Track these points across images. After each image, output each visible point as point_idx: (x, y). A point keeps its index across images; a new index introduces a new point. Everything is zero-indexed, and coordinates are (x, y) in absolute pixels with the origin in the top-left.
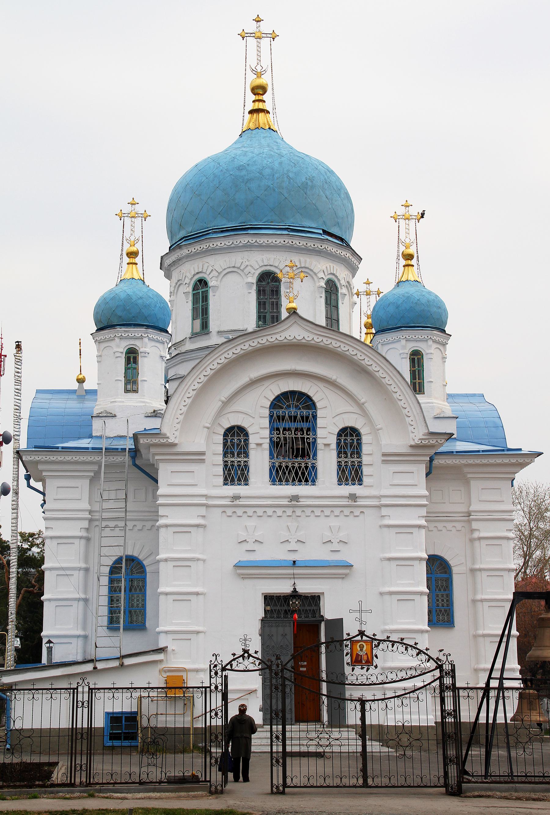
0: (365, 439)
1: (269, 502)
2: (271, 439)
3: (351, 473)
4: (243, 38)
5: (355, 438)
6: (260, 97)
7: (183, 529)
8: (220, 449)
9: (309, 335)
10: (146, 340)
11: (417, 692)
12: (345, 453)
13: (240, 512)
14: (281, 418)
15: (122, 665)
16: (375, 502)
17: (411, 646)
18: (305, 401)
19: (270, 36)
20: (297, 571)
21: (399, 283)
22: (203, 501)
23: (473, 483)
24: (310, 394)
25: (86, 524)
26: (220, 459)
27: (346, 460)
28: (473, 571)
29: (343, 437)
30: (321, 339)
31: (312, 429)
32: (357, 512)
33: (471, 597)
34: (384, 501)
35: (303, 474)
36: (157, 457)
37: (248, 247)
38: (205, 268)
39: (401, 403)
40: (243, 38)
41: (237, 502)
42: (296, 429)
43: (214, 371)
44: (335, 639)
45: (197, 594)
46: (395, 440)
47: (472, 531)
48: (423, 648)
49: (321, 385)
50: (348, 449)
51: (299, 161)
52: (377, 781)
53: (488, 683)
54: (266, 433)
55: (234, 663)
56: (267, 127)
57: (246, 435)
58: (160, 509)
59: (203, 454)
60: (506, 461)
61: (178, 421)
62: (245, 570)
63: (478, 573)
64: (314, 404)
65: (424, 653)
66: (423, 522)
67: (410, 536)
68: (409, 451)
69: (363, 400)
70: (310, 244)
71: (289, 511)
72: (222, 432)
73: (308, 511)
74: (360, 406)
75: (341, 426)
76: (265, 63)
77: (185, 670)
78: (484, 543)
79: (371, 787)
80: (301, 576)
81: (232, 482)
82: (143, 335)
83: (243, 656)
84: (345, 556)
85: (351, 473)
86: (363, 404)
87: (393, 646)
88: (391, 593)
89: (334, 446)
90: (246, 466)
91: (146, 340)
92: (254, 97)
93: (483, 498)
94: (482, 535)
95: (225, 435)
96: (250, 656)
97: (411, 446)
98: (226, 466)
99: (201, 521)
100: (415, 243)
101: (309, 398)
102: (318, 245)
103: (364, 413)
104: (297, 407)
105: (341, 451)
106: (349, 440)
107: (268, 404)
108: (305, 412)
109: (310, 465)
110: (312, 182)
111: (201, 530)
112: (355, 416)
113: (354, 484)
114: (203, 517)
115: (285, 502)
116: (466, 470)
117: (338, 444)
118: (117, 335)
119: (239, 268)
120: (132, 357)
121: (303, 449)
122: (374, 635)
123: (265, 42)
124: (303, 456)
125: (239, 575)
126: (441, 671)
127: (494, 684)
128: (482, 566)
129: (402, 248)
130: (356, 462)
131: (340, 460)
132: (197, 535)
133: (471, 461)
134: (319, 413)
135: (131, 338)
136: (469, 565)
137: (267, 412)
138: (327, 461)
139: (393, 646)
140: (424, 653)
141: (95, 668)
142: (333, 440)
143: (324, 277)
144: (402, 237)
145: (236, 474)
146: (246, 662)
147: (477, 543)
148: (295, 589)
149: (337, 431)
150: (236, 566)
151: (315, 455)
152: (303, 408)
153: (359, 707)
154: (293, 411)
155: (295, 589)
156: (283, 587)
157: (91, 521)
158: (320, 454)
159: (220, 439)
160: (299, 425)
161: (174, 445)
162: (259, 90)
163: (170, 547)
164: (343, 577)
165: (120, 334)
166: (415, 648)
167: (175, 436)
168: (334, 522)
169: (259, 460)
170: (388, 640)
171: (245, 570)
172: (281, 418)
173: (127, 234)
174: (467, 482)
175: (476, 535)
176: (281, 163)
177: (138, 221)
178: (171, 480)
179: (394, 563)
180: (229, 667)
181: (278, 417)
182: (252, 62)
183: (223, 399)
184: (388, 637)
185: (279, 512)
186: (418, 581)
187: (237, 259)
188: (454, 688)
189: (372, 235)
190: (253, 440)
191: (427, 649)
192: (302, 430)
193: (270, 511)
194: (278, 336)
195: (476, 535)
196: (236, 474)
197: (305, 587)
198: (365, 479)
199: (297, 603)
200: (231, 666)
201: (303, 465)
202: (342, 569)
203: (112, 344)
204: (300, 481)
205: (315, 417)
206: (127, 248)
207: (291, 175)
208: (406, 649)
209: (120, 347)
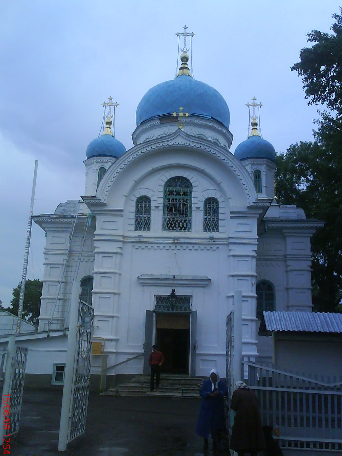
3: (211, 224)
4: (178, 36)
6: (185, 62)
7: (108, 255)
8: (133, 209)
9: (187, 142)
12: (209, 213)
13: (143, 246)
14: (170, 193)
16: (225, 242)
18: (185, 182)
19: (191, 35)
20: (175, 282)
21: (248, 138)
26: (133, 215)
27: (209, 217)
32: (214, 247)
34: (231, 241)
35: (183, 225)
38: (150, 137)
39: (242, 182)
40: (178, 36)
43: (130, 162)
47: (287, 266)
49: (195, 173)
50: (210, 211)
54: (162, 200)
56: (188, 75)
59: (121, 210)
61: (107, 190)
62: (145, 281)
70: (204, 122)
71: (173, 247)
73: (185, 246)
74: (218, 185)
77: (103, 339)
81: (140, 229)
82: (108, 160)
85: (211, 224)
86: (220, 184)
89: (202, 208)
97: (249, 208)
98: (137, 220)
99: (119, 251)
100: (258, 118)
101: (188, 180)
103: (221, 190)
104: (180, 186)
105: (207, 211)
106: (211, 205)
108: (185, 189)
109: (187, 220)
111: (119, 256)
112: (217, 191)
115: (170, 241)
116: (284, 231)
117: (205, 207)
118: (95, 160)
121: (183, 211)
123: (188, 38)
124: (183, 214)
125: (141, 283)
129: (251, 121)
130: (215, 219)
134: (194, 189)
135: (102, 162)
137: (162, 189)
138: (197, 218)
141: (48, 336)
142: (201, 205)
144: (252, 115)
145: (143, 223)
150: (139, 278)
151: (191, 213)
154: (178, 189)
156: (166, 292)
158: (193, 213)
159: (134, 203)
161: (104, 205)
162: (185, 59)
164: (204, 286)
165: (96, 160)
167: (104, 199)
169: (157, 217)
172: (170, 193)
173: (107, 113)
174: (284, 238)
175: (289, 268)
176: (190, 84)
178: (103, 226)
179: (236, 278)
181: (169, 192)
182: (182, 46)
183: (136, 180)
185: (167, 246)
186: (249, 290)
190: (153, 204)
193: (161, 246)
195: (289, 268)
196: (143, 223)
197: (180, 292)
198: (220, 229)
199: (174, 300)
201: (183, 220)
203: (93, 166)
204: (181, 229)
205: (191, 192)
206: (106, 120)
209: (96, 167)
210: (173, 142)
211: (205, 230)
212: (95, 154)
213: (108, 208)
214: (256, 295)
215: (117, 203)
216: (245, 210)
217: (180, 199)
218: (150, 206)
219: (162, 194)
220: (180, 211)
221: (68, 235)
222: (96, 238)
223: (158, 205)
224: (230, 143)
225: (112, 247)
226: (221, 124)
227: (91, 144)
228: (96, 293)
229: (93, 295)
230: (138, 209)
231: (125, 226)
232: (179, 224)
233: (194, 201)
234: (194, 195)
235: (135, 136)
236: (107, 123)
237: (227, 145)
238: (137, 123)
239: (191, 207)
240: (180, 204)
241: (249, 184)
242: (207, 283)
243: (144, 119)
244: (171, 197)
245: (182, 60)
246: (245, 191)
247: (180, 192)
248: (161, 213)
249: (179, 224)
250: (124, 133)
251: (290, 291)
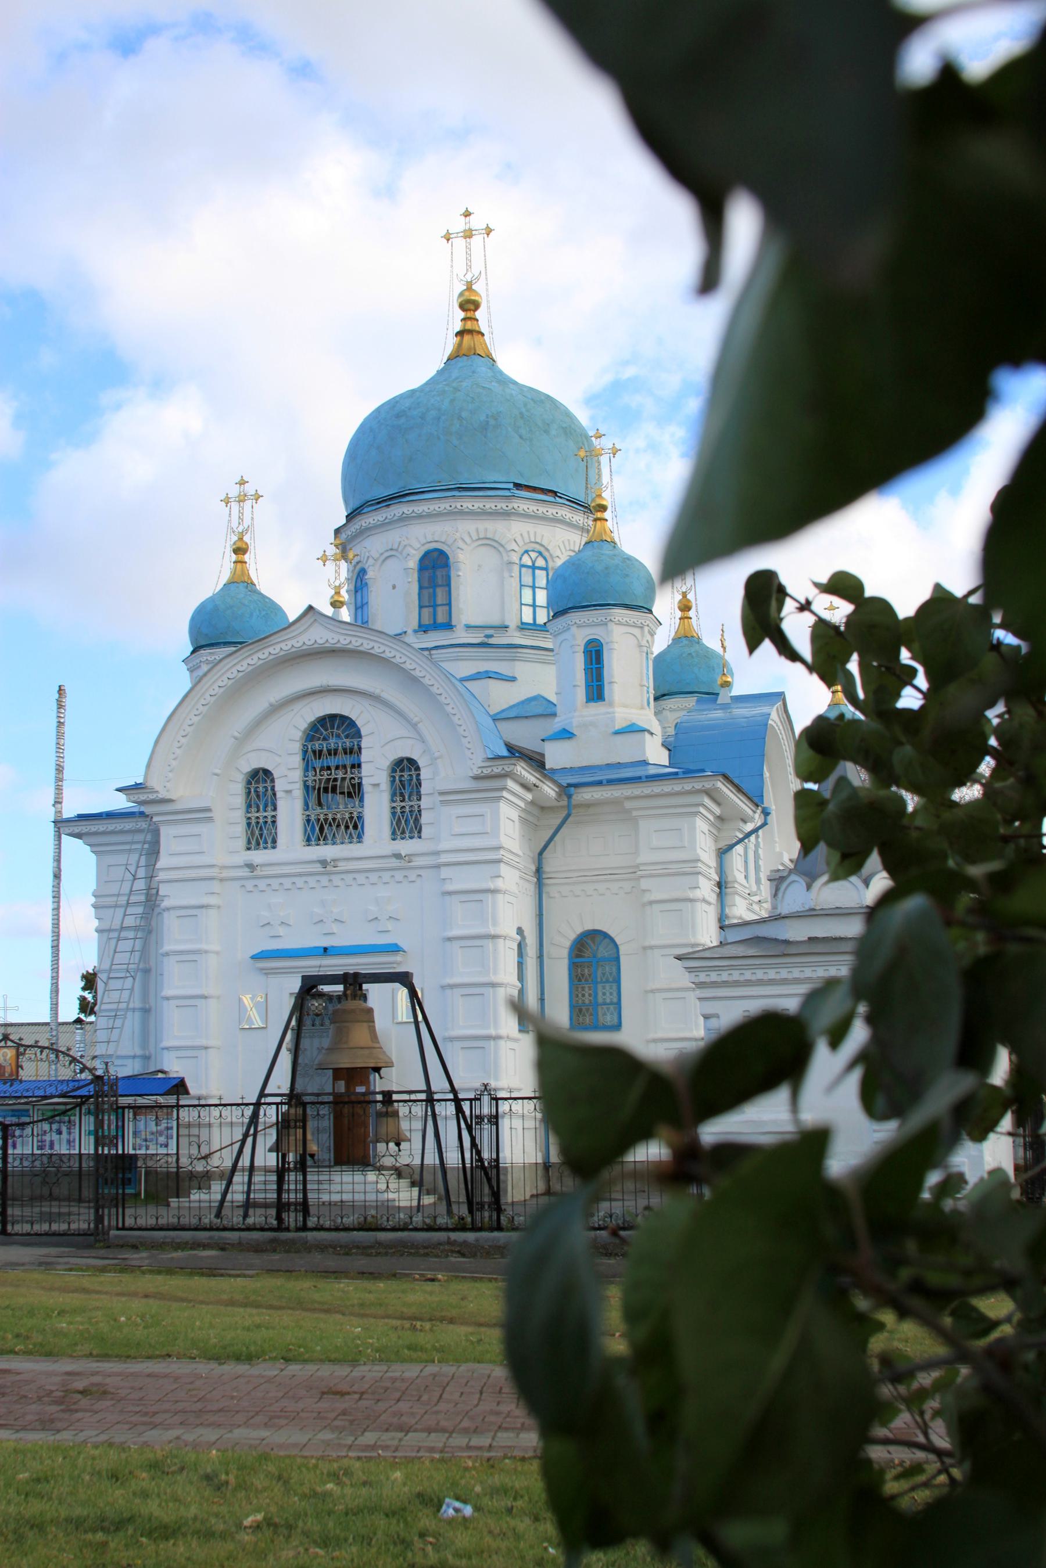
3: (406, 822)
8: (240, 801)
9: (333, 635)
12: (402, 795)
17: (63, 1052)
27: (403, 804)
29: (398, 773)
34: (444, 858)
37: (404, 519)
42: (337, 768)
48: (78, 1055)
52: (18, 1228)
58: (161, 886)
63: (649, 952)
69: (416, 719)
71: (324, 880)
78: (656, 907)
79: (10, 1235)
85: (406, 822)
87: (42, 1052)
90: (360, 818)
91: (574, 629)
92: (462, 315)
94: (654, 896)
97: (476, 778)
102: (502, 505)
104: (338, 736)
106: (405, 774)
109: (355, 815)
110: (496, 419)
113: (411, 838)
116: (628, 805)
119: (397, 550)
120: (595, 656)
122: (20, 1039)
128: (653, 943)
131: (394, 805)
138: (376, 807)
139: (42, 1052)
140: (79, 1062)
143: (516, 548)
145: (261, 833)
152: (347, 737)
154: (332, 742)
162: (469, 305)
169: (290, 812)
170: (35, 1046)
178: (174, 843)
184: (37, 1042)
187: (393, 537)
192: (345, 767)
194: (294, 642)
196: (261, 833)
198: (425, 832)
207: (464, 414)
208: (57, 1057)
212: (204, 643)
213: (178, 806)
219: (297, 760)
223: (289, 787)
231: (223, 839)
233: (365, 770)
245: (462, 307)
246: (463, 739)
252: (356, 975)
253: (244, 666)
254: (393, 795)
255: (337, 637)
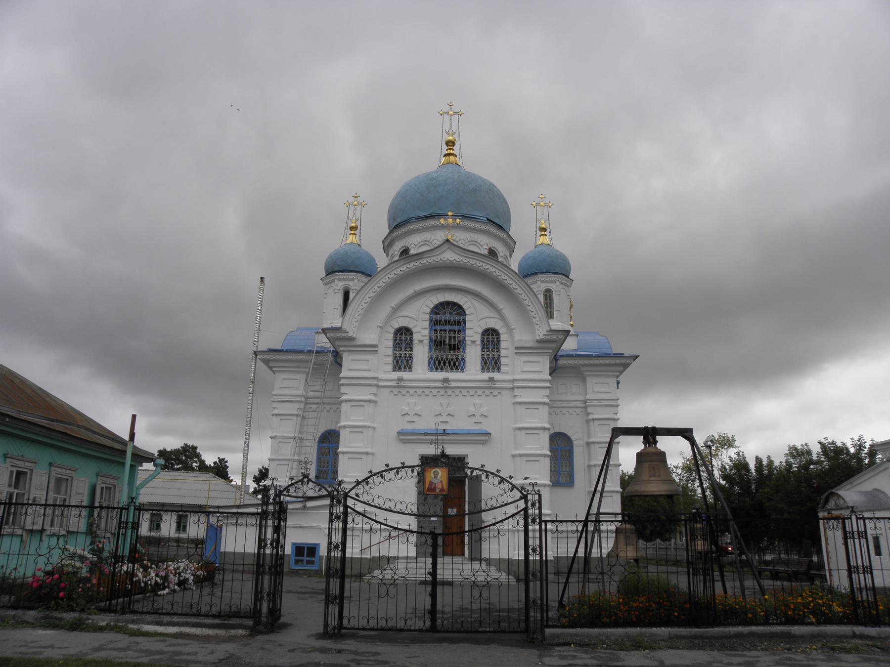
0: (502, 337)
1: (427, 384)
2: (430, 337)
3: (491, 363)
5: (495, 337)
7: (359, 403)
8: (391, 344)
10: (356, 281)
11: (498, 525)
13: (404, 391)
14: (438, 322)
15: (305, 507)
17: (492, 474)
18: (458, 309)
20: (445, 438)
22: (375, 382)
23: (588, 379)
24: (461, 303)
25: (302, 406)
26: (390, 351)
28: (588, 444)
30: (468, 260)
31: (462, 331)
32: (495, 392)
33: (586, 464)
35: (454, 364)
36: (341, 349)
41: (402, 384)
44: (406, 464)
45: (367, 453)
46: (523, 337)
47: (588, 414)
48: (505, 475)
49: (469, 297)
51: (470, 176)
53: (587, 517)
54: (427, 332)
55: (292, 490)
57: (411, 334)
59: (376, 346)
60: (613, 362)
62: (405, 437)
64: (464, 311)
65: (508, 482)
66: (546, 400)
67: (536, 411)
68: (536, 345)
70: (478, 226)
71: (442, 392)
72: (393, 331)
73: (457, 391)
74: (499, 311)
75: (485, 327)
76: (455, 128)
78: (596, 422)
80: (354, 382)
81: (400, 369)
83: (302, 481)
84: (484, 427)
85: (491, 363)
88: (521, 455)
89: (479, 342)
93: (597, 390)
94: (596, 416)
95: (395, 334)
96: (309, 480)
97: (538, 341)
98: (395, 357)
99: (372, 398)
101: (460, 307)
103: (502, 318)
104: (451, 314)
105: (485, 346)
106: (491, 338)
107: (429, 311)
108: (457, 318)
109: (460, 357)
111: (372, 404)
112: (495, 320)
114: (375, 395)
116: (583, 369)
117: (482, 341)
124: (454, 349)
126: (526, 503)
127: (592, 518)
128: (595, 440)
132: (369, 408)
133: (586, 362)
136: (586, 440)
137: (427, 317)
138: (473, 354)
140: (508, 482)
142: (478, 338)
145: (403, 362)
146: (305, 488)
147: (591, 424)
148: (443, 451)
149: (481, 331)
150: (399, 433)
151: (464, 349)
153: (430, 542)
154: (448, 317)
155: (443, 451)
157: (306, 404)
158: (468, 349)
159: (391, 336)
160: (452, 328)
161: (352, 339)
162: (450, 144)
163: (349, 418)
164: (484, 443)
166: (497, 476)
168: (477, 400)
169: (421, 353)
171: (405, 437)
172: (438, 322)
173: (351, 216)
174: (584, 379)
175: (591, 417)
177: (358, 208)
178: (351, 365)
180: (285, 493)
185: (435, 392)
186: (542, 446)
188: (540, 519)
189: (522, 228)
190: (416, 337)
191: (511, 477)
193: (427, 391)
194: (435, 258)
195: (591, 417)
196: (403, 362)
198: (502, 368)
200: (288, 492)
201: (454, 357)
202: (483, 438)
204: (452, 369)
205: (464, 321)
208: (382, 477)
210: (439, 257)
211: (483, 370)
213: (357, 342)
214: (548, 453)
215: (368, 336)
216: (531, 344)
217: (450, 331)
218: (411, 340)
219: (427, 324)
220: (450, 345)
221: (304, 376)
222: (342, 382)
223: (422, 338)
224: (512, 251)
225: (363, 394)
226: (500, 227)
227: (330, 256)
228: (344, 453)
229: (340, 456)
230: (397, 345)
231: (380, 366)
232: (449, 363)
233: (468, 332)
234: (468, 325)
235: (388, 245)
236: (352, 228)
237: (508, 254)
238: (389, 226)
239: (464, 340)
240: (450, 337)
241: (537, 311)
242: (486, 438)
243: (398, 221)
244: (438, 328)
247: (449, 321)
248: (426, 348)
249: (449, 363)
250: (372, 240)
251: (592, 445)
252: (654, 428)
253: (404, 268)
254: (483, 348)
255: (461, 258)
